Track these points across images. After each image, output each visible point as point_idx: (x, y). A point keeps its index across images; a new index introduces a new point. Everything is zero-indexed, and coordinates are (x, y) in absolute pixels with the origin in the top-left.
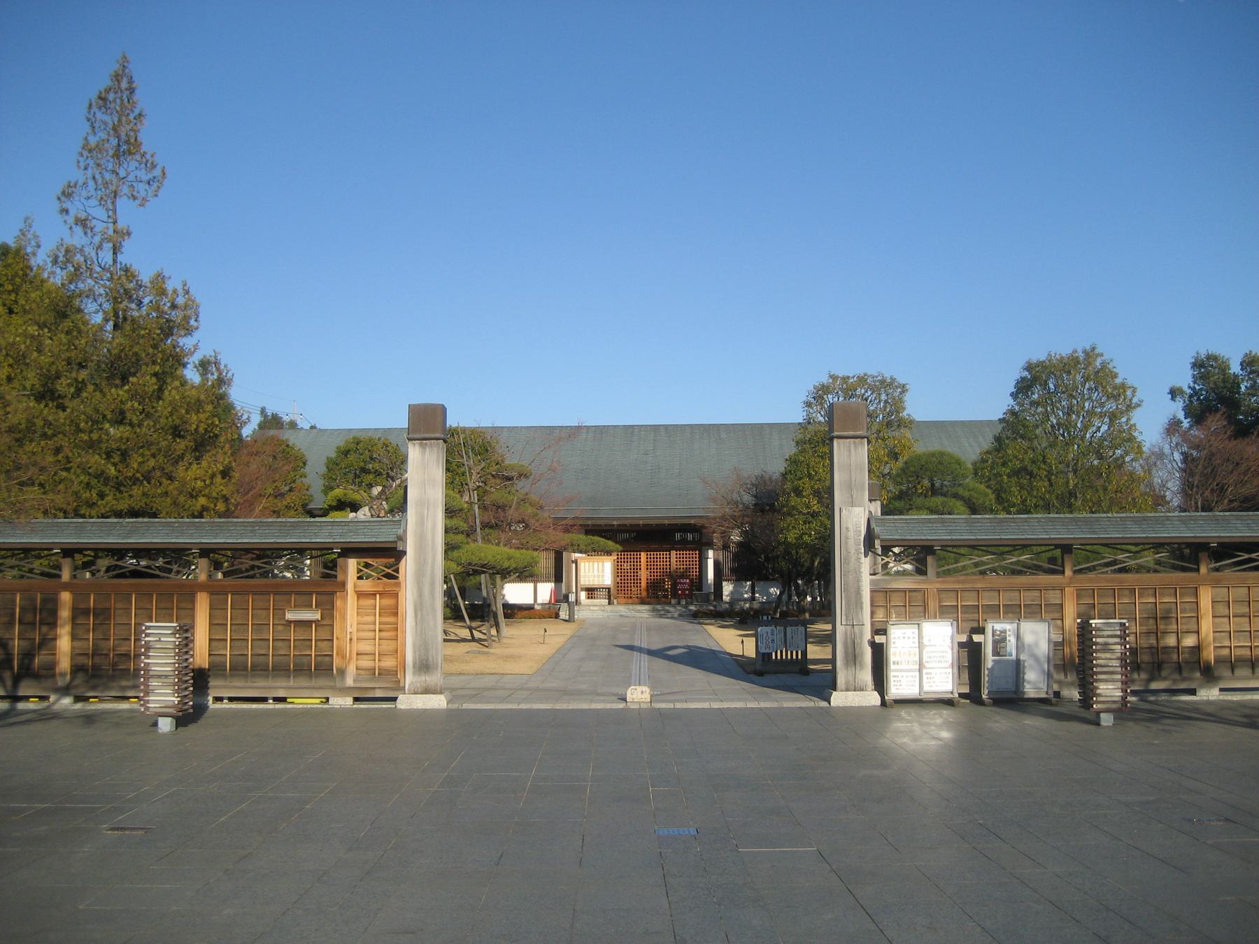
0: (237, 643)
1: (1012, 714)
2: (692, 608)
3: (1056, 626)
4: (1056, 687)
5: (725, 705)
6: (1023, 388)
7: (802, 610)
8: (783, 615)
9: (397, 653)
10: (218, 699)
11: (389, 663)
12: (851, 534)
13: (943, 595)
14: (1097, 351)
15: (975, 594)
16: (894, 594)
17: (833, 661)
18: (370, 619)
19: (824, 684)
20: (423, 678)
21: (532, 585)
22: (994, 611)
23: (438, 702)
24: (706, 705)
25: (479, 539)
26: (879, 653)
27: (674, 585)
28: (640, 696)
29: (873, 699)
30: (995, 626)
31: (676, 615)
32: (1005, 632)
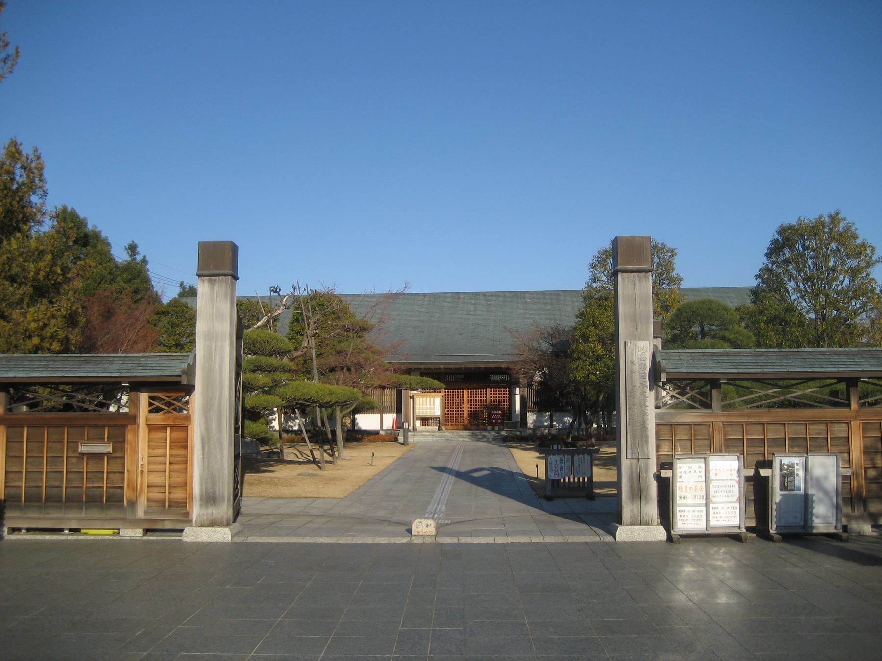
0: (32, 475)
1: (807, 553)
2: (503, 433)
3: (843, 460)
4: (844, 521)
5: (510, 540)
6: (775, 249)
7: (589, 436)
8: (575, 439)
9: (185, 485)
10: (13, 530)
11: (178, 495)
12: (636, 367)
13: (729, 429)
14: (840, 216)
15: (760, 428)
16: (681, 428)
17: (617, 485)
18: (161, 451)
19: (610, 518)
20: (210, 511)
21: (378, 416)
22: (780, 444)
23: (223, 535)
24: (489, 540)
25: (316, 377)
26: (665, 490)
27: (490, 415)
28: (425, 529)
29: (659, 533)
30: (782, 460)
31: (490, 439)
32: (791, 466)
